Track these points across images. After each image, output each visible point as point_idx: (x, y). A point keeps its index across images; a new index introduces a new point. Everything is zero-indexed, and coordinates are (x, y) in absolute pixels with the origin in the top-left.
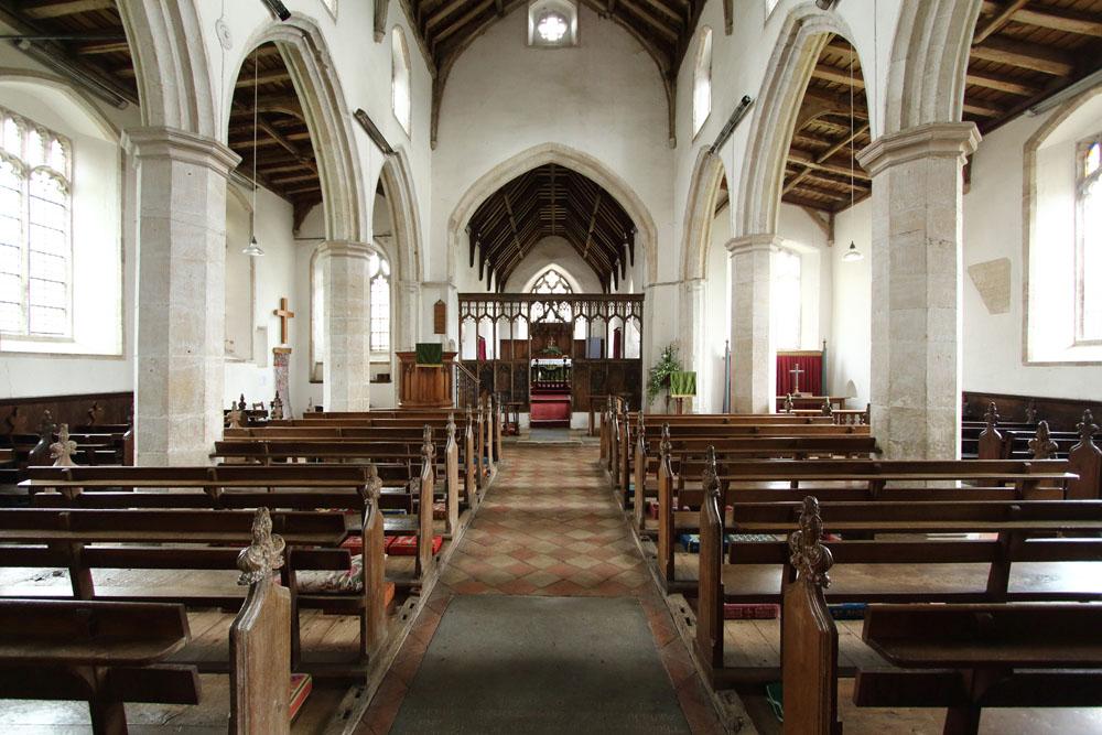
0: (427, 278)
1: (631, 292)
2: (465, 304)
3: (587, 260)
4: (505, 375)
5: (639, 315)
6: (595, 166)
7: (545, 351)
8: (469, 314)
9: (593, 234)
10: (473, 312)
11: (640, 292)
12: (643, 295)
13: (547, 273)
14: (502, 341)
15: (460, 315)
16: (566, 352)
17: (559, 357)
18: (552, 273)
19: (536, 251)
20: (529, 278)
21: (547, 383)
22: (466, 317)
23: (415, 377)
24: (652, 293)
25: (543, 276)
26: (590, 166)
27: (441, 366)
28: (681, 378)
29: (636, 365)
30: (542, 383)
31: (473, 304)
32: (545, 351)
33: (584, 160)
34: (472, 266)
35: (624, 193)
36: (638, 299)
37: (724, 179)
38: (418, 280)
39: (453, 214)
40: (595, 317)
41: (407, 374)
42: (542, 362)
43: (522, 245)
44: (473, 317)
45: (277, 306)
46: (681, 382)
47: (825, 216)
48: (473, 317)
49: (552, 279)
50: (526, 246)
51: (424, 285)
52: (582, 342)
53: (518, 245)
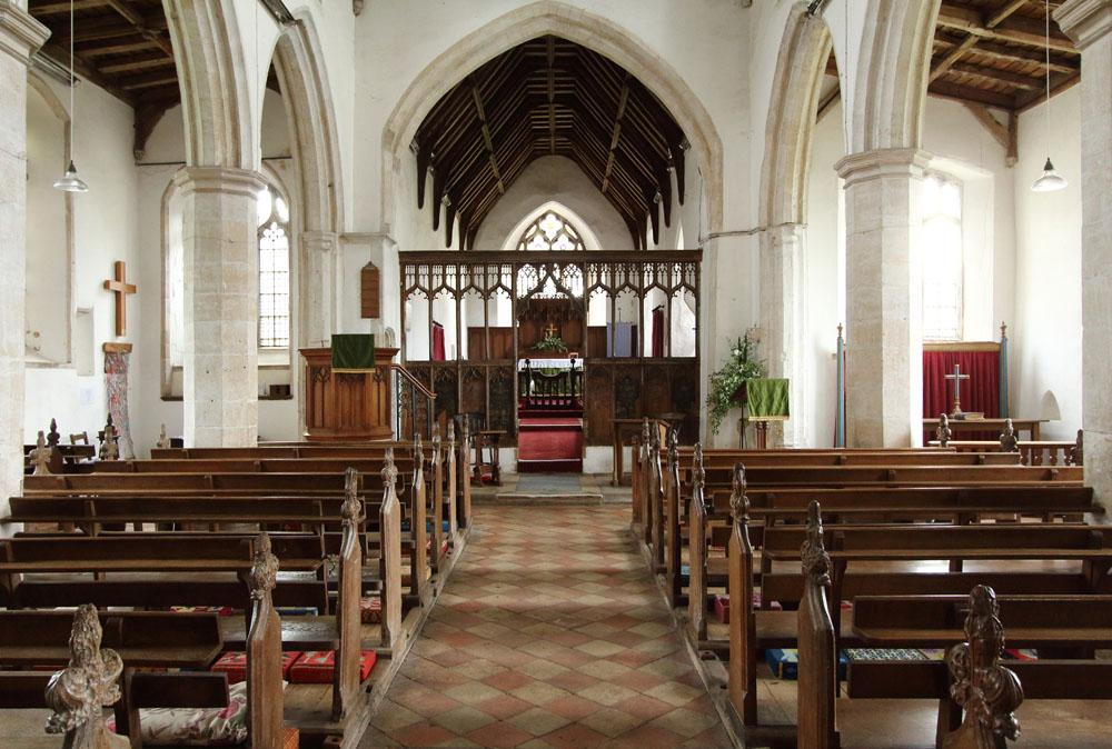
1: (680, 246)
2: (410, 270)
3: (608, 194)
4: (476, 386)
5: (693, 284)
6: (619, 39)
8: (417, 286)
9: (617, 151)
10: (424, 282)
11: (696, 247)
12: (700, 252)
13: (543, 217)
14: (469, 329)
15: (403, 287)
16: (574, 348)
17: (564, 356)
18: (551, 218)
19: (522, 182)
20: (514, 225)
21: (543, 399)
22: (412, 290)
23: (330, 390)
24: (714, 249)
26: (611, 39)
27: (372, 371)
28: (764, 389)
29: (693, 364)
30: (536, 399)
31: (424, 270)
33: (600, 28)
34: (421, 205)
35: (667, 84)
36: (692, 258)
37: (832, 58)
38: (334, 231)
39: (390, 121)
40: (622, 288)
41: (318, 385)
42: (536, 363)
43: (501, 171)
45: (109, 275)
46: (765, 395)
47: (1001, 116)
48: (423, 290)
50: (509, 173)
51: (344, 237)
52: (602, 330)
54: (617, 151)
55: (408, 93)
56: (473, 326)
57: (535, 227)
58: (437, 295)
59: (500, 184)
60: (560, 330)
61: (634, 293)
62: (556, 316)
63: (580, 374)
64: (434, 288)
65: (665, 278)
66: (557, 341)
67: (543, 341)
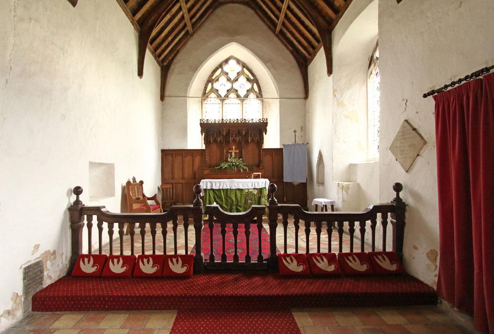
3: (281, 36)
7: (224, 165)
13: (226, 61)
18: (232, 62)
25: (220, 66)
32: (224, 165)
34: (140, 73)
49: (232, 68)
52: (279, 152)
56: (166, 148)
57: (220, 70)
60: (241, 152)
62: (237, 139)
66: (238, 162)
67: (227, 161)
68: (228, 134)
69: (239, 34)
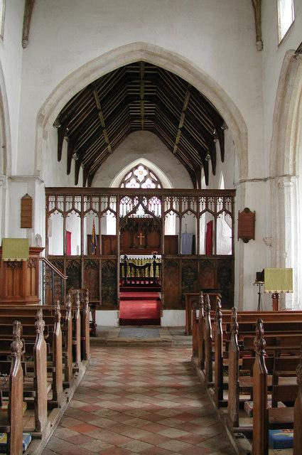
0: (15, 172)
1: (222, 187)
2: (52, 199)
3: (177, 155)
4: (93, 272)
5: (115, 210)
6: (184, 65)
9: (183, 129)
10: (61, 206)
13: (136, 167)
15: (47, 209)
18: (141, 168)
19: (125, 145)
22: (168, 211)
25: (132, 171)
31: (60, 199)
33: (171, 57)
34: (59, 159)
35: (214, 91)
39: (42, 109)
40: (186, 212)
43: (110, 139)
44: (60, 211)
50: (115, 140)
51: (11, 178)
52: (175, 237)
53: (107, 140)
54: (183, 129)
55: (53, 92)
58: (69, 214)
59: (109, 147)
61: (193, 215)
63: (159, 264)
64: (67, 210)
65: (230, 206)
68: (137, 225)
69: (146, 152)
